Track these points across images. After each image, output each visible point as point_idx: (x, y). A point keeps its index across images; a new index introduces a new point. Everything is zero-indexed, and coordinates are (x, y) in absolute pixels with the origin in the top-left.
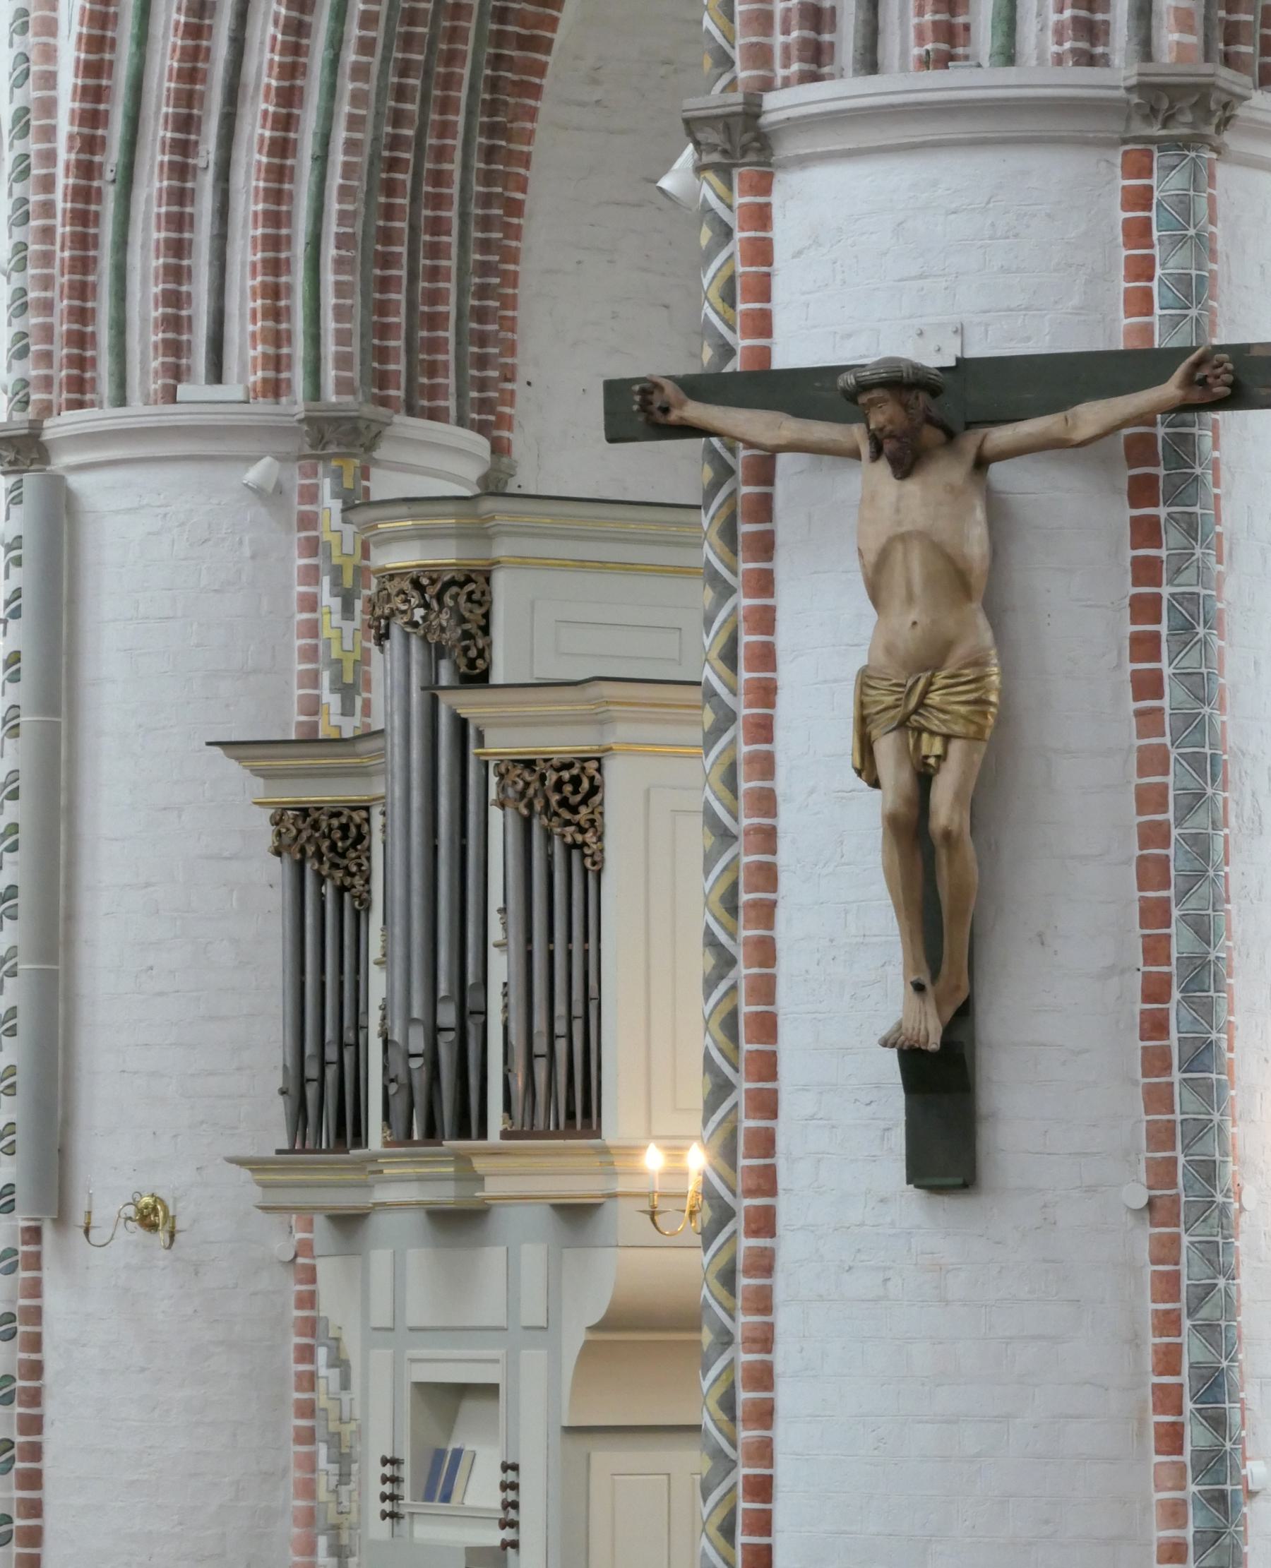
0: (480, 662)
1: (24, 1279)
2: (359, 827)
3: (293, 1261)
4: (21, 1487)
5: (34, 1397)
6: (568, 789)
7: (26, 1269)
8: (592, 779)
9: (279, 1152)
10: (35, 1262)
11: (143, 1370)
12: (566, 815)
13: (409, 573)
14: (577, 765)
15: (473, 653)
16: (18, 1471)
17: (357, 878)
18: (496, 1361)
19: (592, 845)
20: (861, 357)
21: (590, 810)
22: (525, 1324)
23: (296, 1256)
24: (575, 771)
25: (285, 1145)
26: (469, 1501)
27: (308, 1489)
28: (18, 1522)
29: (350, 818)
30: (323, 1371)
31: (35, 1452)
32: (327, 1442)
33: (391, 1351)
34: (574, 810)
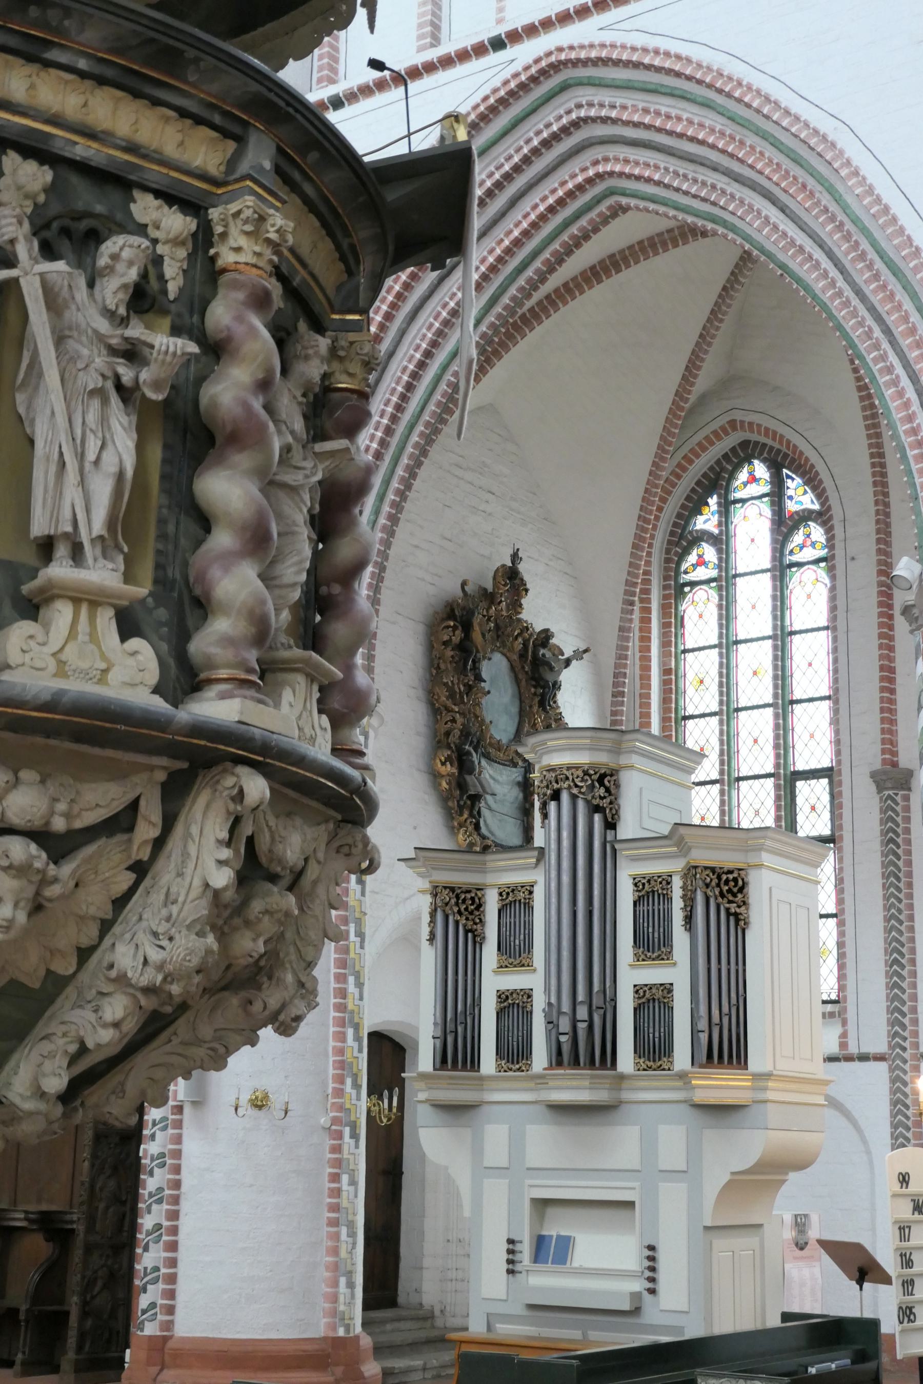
1: (172, 1134)
2: (479, 899)
4: (166, 1250)
5: (176, 1200)
7: (174, 1128)
8: (743, 880)
10: (179, 1124)
11: (251, 1186)
12: (731, 898)
14: (736, 872)
15: (614, 812)
16: (165, 1242)
18: (634, 1189)
22: (529, 1165)
24: (735, 875)
25: (546, 1066)
27: (335, 1251)
28: (163, 1271)
29: (476, 894)
31: (174, 1231)
32: (347, 1226)
33: (507, 1181)
34: (735, 895)
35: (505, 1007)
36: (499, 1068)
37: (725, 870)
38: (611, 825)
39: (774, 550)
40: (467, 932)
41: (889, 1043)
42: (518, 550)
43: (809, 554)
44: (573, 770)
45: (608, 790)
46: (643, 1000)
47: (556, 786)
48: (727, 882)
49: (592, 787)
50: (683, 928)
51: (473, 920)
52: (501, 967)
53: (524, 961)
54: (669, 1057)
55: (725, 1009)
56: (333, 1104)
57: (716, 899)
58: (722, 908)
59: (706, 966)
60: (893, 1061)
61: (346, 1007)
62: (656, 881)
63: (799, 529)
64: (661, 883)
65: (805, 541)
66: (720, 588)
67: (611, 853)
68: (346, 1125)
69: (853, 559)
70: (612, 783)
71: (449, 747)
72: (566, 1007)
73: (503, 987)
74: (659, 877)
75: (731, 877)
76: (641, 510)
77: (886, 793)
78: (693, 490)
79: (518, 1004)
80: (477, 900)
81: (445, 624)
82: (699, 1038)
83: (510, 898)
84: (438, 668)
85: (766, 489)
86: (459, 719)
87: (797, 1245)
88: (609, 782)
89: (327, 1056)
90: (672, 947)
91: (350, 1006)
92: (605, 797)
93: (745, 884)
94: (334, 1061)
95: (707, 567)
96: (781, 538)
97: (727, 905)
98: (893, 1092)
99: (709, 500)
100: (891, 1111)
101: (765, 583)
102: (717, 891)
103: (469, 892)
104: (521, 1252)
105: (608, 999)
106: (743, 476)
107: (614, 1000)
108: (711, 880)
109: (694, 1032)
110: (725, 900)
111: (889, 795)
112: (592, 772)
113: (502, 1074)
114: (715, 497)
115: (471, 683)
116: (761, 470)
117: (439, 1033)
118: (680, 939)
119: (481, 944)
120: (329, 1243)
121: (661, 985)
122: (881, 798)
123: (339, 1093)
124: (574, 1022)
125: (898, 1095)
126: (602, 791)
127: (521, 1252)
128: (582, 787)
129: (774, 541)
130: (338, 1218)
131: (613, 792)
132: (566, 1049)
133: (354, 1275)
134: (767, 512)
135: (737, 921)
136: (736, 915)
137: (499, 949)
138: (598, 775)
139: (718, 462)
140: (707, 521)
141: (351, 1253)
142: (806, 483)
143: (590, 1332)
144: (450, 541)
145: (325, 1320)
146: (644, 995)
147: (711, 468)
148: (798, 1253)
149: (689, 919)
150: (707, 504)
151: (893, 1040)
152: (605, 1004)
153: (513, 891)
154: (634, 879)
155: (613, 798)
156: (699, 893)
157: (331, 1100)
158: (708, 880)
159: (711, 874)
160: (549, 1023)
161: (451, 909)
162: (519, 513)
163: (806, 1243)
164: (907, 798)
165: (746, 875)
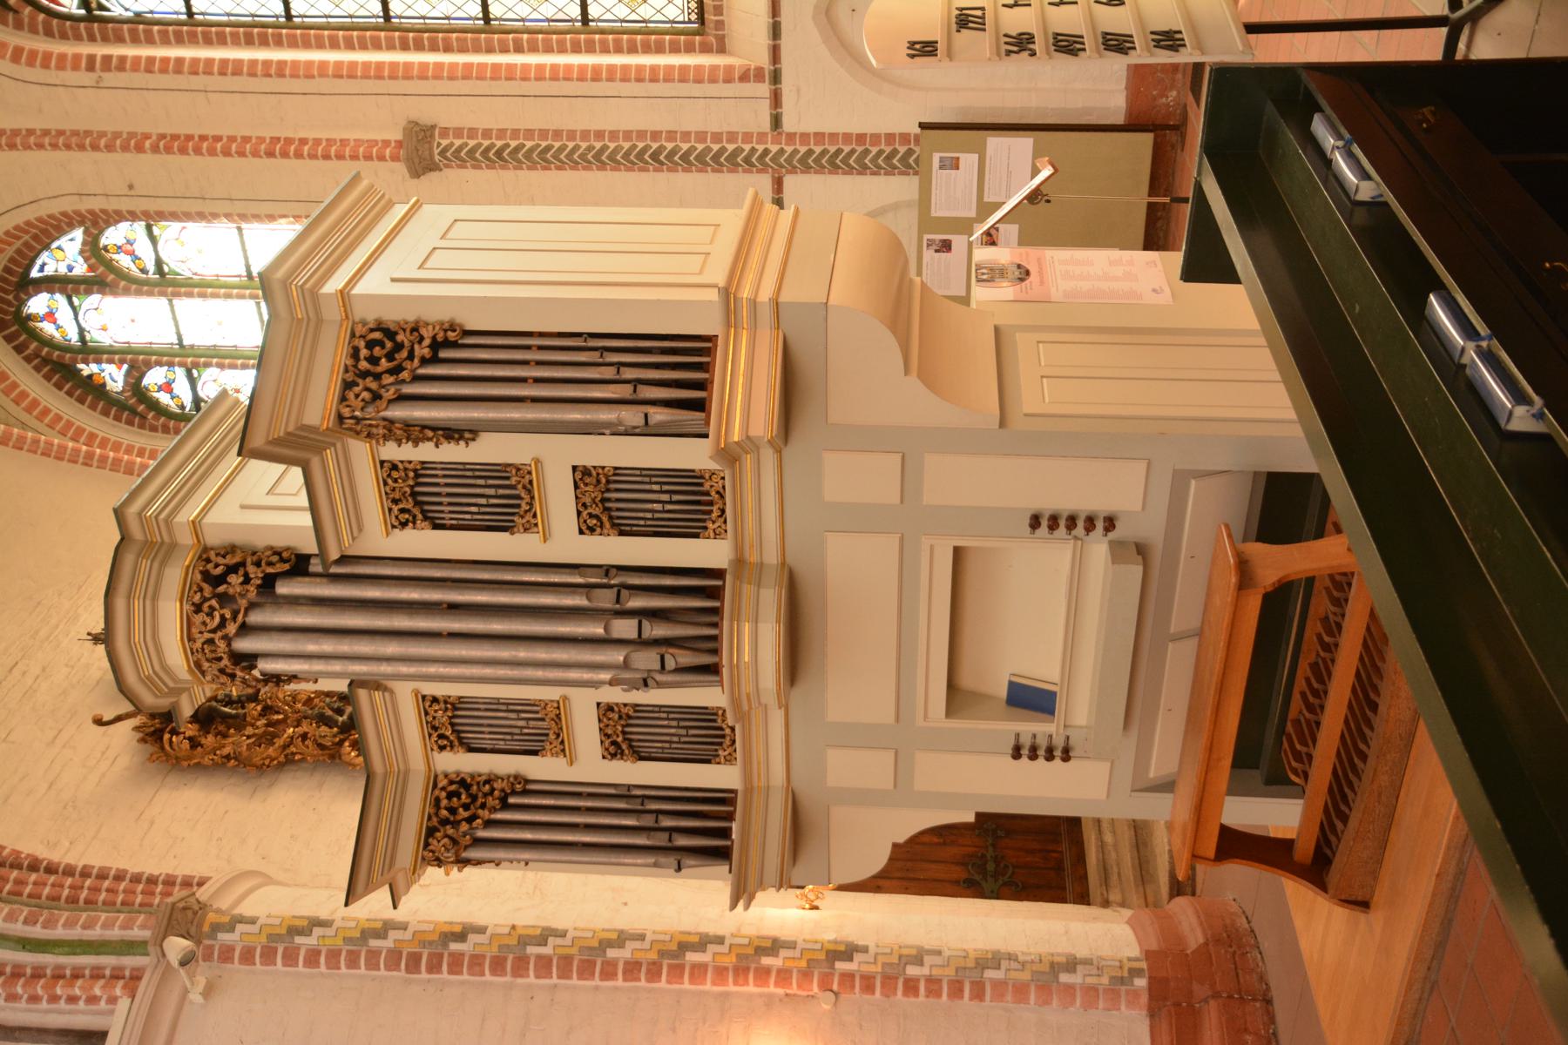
0: (285, 555)
2: (451, 782)
3: (836, 994)
6: (377, 351)
8: (372, 330)
9: (730, 872)
12: (404, 354)
13: (188, 616)
17: (495, 785)
18: (932, 547)
19: (436, 331)
20: (366, 903)
21: (401, 332)
23: (832, 991)
24: (362, 344)
26: (1056, 677)
29: (443, 789)
30: (925, 971)
34: (399, 347)
35: (631, 747)
36: (730, 760)
37: (350, 362)
38: (299, 565)
39: (139, 293)
40: (506, 806)
41: (759, 171)
42: (89, 634)
43: (144, 248)
44: (194, 630)
45: (232, 569)
46: (605, 519)
47: (225, 662)
48: (373, 360)
49: (224, 599)
50: (472, 444)
51: (485, 795)
52: (563, 750)
53: (552, 715)
54: (702, 477)
55: (609, 373)
56: (799, 986)
57: (403, 381)
58: (422, 371)
59: (530, 405)
60: (782, 166)
61: (654, 963)
62: (394, 490)
63: (112, 260)
64: (395, 481)
65: (127, 253)
66: (196, 365)
67: (351, 567)
68: (832, 967)
69: (131, 187)
70: (220, 560)
71: (341, 743)
72: (618, 656)
73: (598, 750)
74: (385, 484)
75: (364, 352)
76: (75, 462)
77: (437, 158)
78: (70, 394)
79: (623, 726)
80: (453, 787)
81: (167, 746)
82: (660, 424)
83: (448, 733)
84: (228, 757)
85: (60, 299)
86: (304, 728)
87: (1022, 280)
88: (217, 566)
89: (726, 995)
90: (510, 465)
91: (653, 956)
92: (246, 575)
93: (380, 327)
94: (736, 983)
95: (174, 381)
96: (123, 283)
97: (416, 361)
98: (821, 169)
99: (85, 373)
100: (845, 173)
101: (187, 307)
102: (387, 379)
103: (438, 800)
104: (1034, 736)
105: (605, 581)
106: (47, 328)
107: (607, 570)
108: (367, 389)
109: (648, 430)
110: (407, 364)
111: (439, 154)
112: (197, 598)
113: (739, 755)
114: (81, 366)
115: (259, 708)
116: (37, 304)
117: (671, 860)
118: (489, 450)
119: (527, 781)
120: (1009, 997)
121: (576, 487)
122: (447, 166)
123: (784, 976)
124: (641, 643)
125: (823, 161)
126: (235, 579)
127: (1034, 736)
128: (223, 617)
129: (126, 292)
130: (972, 983)
131: (237, 559)
132: (686, 658)
133: (1057, 959)
134: (94, 299)
135: (447, 344)
136: (436, 345)
137: (535, 753)
138: (205, 586)
139: (28, 359)
140: (114, 377)
141: (1024, 964)
142: (47, 247)
143: (1172, 630)
144: (60, 731)
145: (1123, 1007)
146: (597, 517)
147: (37, 369)
148: (1034, 277)
149: (452, 433)
150: (90, 377)
151: (755, 166)
152: (612, 586)
153: (435, 728)
154: (394, 527)
155: (249, 561)
156: (389, 414)
157: (794, 990)
158: (366, 395)
159: (357, 389)
160: (646, 685)
161: (465, 834)
162: (57, 626)
163: (1019, 266)
164: (445, 132)
165: (364, 323)
